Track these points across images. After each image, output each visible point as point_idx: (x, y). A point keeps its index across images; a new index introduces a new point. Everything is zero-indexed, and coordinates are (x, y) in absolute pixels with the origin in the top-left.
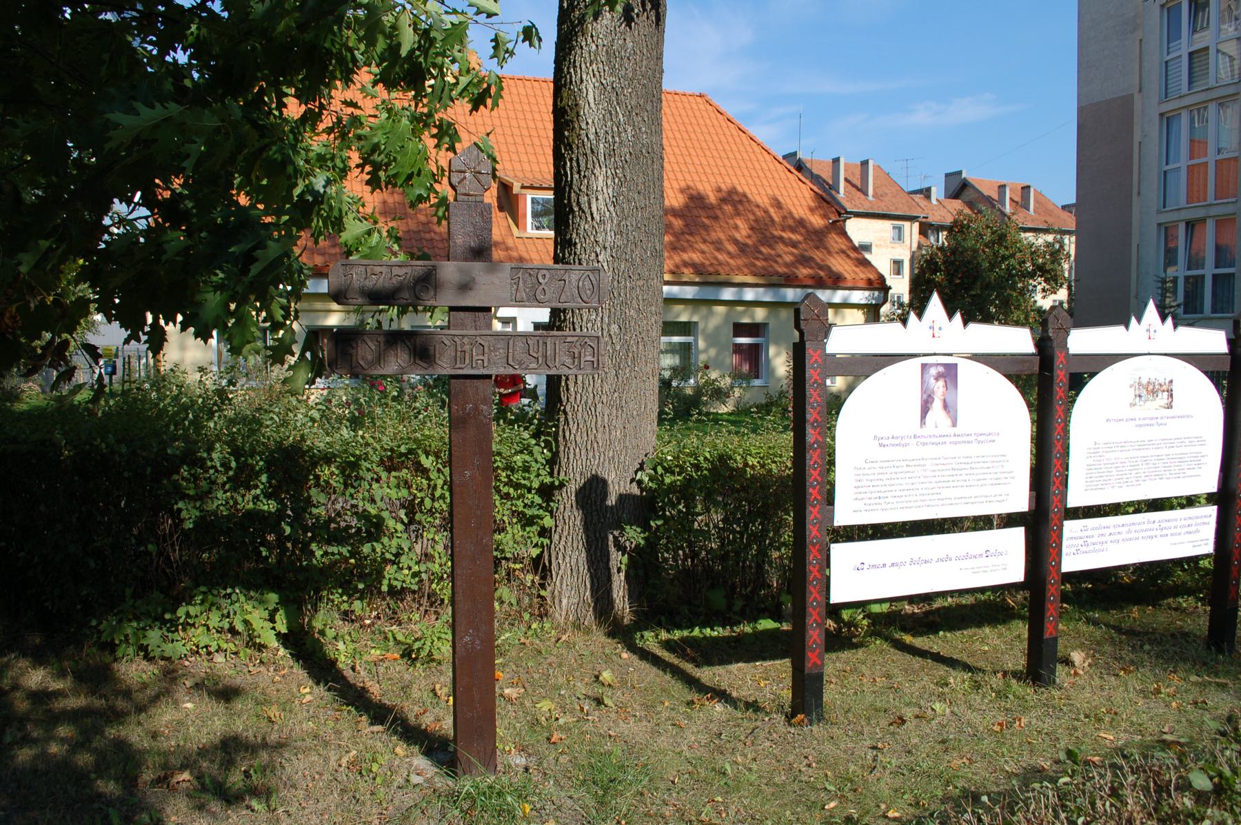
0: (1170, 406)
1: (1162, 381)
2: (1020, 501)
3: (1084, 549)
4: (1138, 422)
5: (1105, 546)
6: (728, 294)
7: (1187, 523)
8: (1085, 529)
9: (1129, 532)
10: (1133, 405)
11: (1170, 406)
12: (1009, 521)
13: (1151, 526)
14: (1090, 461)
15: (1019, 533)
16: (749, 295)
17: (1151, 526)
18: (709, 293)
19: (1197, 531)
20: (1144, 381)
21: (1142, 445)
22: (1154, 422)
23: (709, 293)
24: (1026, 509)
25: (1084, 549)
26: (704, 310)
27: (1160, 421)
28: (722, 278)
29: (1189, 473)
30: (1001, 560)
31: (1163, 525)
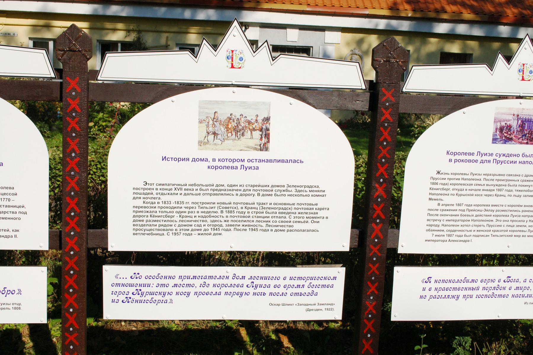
0: (264, 148)
1: (251, 117)
2: (341, 240)
3: (137, 297)
4: (212, 164)
5: (167, 297)
6: (442, 28)
7: (296, 283)
8: (137, 276)
9: (204, 285)
10: (495, 140)
11: (264, 148)
12: (32, 258)
13: (240, 282)
14: (139, 202)
15: (339, 273)
16: (462, 29)
17: (240, 282)
18: (423, 28)
19: (313, 294)
20: (223, 117)
21: (218, 190)
22: (239, 164)
23: (423, 28)
24: (347, 249)
25: (137, 297)
26: (418, 42)
27: (246, 164)
28: (432, 15)
29: (297, 226)
30: (321, 298)
31: (256, 282)
